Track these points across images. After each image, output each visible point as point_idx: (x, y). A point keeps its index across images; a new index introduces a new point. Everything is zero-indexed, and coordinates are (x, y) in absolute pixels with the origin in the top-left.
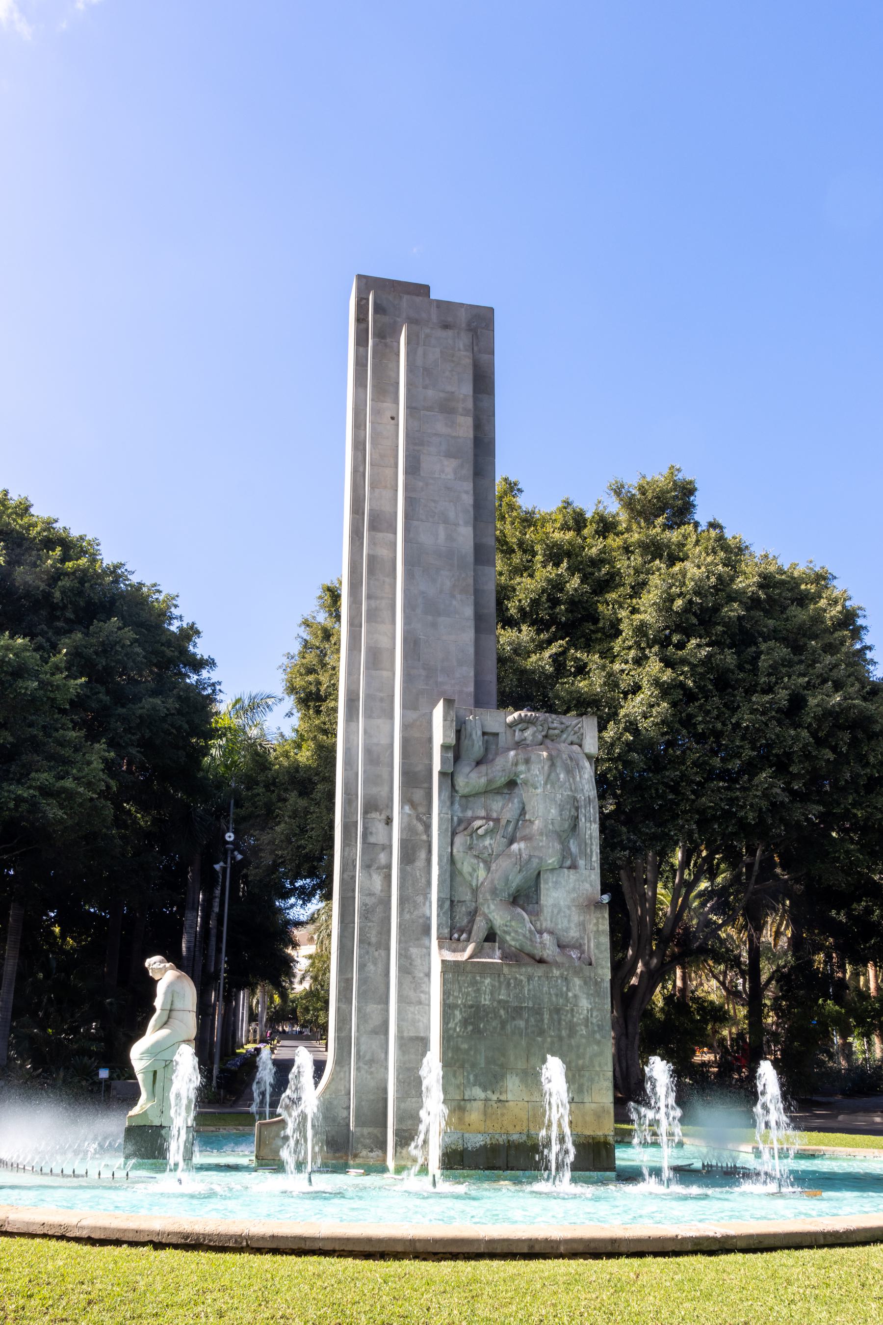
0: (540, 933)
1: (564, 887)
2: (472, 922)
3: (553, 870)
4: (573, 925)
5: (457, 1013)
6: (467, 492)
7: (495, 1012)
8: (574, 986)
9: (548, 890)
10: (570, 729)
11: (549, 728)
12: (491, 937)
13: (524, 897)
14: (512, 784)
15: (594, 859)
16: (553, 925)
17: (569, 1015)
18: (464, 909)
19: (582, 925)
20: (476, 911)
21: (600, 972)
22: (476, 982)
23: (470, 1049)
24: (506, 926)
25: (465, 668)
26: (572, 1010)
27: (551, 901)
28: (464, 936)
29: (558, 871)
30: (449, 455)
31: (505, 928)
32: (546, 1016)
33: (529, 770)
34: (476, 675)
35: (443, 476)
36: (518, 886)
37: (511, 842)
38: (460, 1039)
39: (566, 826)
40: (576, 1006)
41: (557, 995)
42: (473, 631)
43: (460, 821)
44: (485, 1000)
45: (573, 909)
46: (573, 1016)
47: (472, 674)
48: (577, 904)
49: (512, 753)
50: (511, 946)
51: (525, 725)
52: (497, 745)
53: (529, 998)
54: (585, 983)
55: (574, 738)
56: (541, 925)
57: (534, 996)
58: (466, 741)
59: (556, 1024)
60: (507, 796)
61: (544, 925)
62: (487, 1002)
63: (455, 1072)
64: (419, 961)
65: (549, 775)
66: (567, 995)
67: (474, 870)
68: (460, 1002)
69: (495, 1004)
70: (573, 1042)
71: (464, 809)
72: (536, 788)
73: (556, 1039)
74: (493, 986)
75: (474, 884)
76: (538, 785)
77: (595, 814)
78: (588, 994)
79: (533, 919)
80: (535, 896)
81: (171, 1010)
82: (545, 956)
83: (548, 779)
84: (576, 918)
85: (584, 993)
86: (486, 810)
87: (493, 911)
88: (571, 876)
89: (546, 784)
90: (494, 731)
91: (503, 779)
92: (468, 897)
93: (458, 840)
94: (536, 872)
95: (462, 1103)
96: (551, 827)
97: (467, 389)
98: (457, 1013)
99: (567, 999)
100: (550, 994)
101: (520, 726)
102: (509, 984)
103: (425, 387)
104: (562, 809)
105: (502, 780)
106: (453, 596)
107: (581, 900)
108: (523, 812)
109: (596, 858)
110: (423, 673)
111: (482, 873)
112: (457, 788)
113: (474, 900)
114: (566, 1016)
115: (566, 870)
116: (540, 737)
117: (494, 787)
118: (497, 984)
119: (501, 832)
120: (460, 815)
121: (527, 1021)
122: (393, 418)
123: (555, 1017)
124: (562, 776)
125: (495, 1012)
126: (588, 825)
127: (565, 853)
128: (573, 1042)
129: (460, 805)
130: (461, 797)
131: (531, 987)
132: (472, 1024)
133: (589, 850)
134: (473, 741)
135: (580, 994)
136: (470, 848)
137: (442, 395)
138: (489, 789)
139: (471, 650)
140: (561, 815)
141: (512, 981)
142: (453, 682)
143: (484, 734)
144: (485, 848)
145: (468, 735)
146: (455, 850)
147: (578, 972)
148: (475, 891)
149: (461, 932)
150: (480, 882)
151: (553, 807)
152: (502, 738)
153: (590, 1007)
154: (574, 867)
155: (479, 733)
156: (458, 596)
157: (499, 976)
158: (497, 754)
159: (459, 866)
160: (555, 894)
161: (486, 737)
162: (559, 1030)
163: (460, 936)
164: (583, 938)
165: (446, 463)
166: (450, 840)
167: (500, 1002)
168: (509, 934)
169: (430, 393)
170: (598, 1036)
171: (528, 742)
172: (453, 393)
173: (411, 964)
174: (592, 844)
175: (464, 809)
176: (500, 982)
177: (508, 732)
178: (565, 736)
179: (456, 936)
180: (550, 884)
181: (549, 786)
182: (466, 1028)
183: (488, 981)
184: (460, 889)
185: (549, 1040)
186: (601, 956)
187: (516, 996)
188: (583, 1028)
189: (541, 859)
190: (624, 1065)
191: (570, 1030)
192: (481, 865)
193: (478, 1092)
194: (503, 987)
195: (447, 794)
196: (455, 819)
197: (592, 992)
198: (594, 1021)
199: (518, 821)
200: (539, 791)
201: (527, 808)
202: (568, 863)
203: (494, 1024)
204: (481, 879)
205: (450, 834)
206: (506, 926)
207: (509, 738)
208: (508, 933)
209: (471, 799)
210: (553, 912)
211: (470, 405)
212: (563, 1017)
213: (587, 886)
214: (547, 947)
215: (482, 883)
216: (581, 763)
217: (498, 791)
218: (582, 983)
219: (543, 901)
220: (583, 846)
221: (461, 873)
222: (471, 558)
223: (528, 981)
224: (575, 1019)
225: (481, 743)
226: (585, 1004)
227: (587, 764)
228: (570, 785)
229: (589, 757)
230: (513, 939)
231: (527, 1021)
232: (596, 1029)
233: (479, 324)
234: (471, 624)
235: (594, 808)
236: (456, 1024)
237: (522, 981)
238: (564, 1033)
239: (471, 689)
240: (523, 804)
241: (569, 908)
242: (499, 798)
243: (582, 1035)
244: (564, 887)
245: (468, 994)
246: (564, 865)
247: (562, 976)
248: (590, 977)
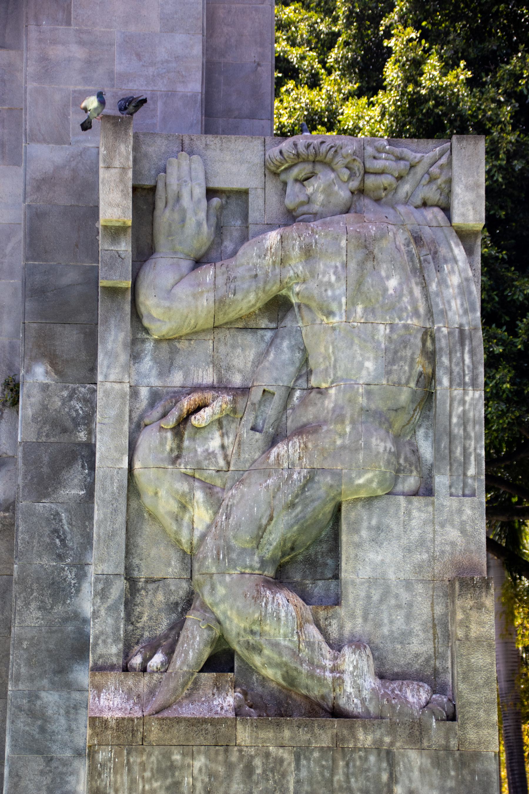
0: (336, 646)
1: (399, 538)
2: (178, 626)
3: (370, 500)
4: (416, 627)
8: (409, 769)
9: (358, 545)
11: (366, 172)
12: (221, 660)
13: (307, 564)
14: (279, 307)
15: (471, 471)
16: (369, 627)
19: (441, 629)
20: (189, 601)
21: (472, 735)
22: (172, 767)
24: (252, 632)
25: (180, 37)
27: (365, 573)
28: (158, 659)
29: (382, 503)
31: (250, 638)
37: (273, 442)
43: (155, 397)
45: (419, 588)
47: (197, 50)
48: (428, 576)
50: (265, 679)
54: (438, 762)
55: (432, 193)
56: (341, 627)
58: (167, 213)
60: (269, 335)
61: (348, 627)
64: (63, 721)
65: (360, 283)
67: (184, 507)
71: (165, 368)
72: (330, 313)
75: (184, 539)
76: (334, 307)
77: (474, 367)
79: (322, 614)
80: (330, 561)
82: (342, 702)
84: (423, 609)
87: (223, 600)
88: (415, 513)
89: (352, 303)
90: (236, 185)
92: (173, 569)
93: (148, 441)
94: (329, 508)
96: (362, 401)
101: (295, 172)
102: (249, 770)
104: (392, 356)
105: (249, 300)
107: (438, 567)
108: (305, 369)
110: (78, 53)
111: (201, 515)
112: (146, 323)
113: (186, 576)
115: (402, 499)
116: (343, 194)
117: (232, 314)
118: (221, 769)
120: (155, 382)
124: (393, 283)
126: (458, 392)
127: (404, 460)
129: (155, 359)
130: (158, 341)
131: (304, 773)
133: (458, 451)
134: (183, 211)
138: (221, 319)
140: (389, 373)
141: (258, 762)
142: (151, 71)
144: (210, 455)
145: (171, 196)
146: (137, 465)
147: (417, 733)
148: (189, 559)
149: (152, 648)
150: (197, 534)
151: (371, 355)
154: (426, 490)
155: (200, 192)
157: (226, 751)
158: (244, 238)
159: (147, 500)
160: (374, 556)
161: (216, 201)
163: (146, 660)
164: (443, 657)
166: (126, 443)
171: (316, 207)
173: (43, 730)
174: (467, 437)
175: (165, 368)
176: (230, 767)
177: (269, 185)
179: (137, 661)
180: (364, 533)
181: (359, 309)
183: (200, 762)
186: (474, 698)
189: (337, 475)
192: (199, 495)
194: (237, 774)
195: (121, 336)
196: (144, 392)
199: (290, 391)
200: (335, 320)
201: (312, 362)
202: (411, 482)
204: (200, 527)
205: (126, 427)
206: (252, 632)
207: (273, 199)
208: (257, 649)
209: (182, 345)
210: (369, 597)
214: (355, 681)
215: (203, 537)
216: (443, 251)
217: (245, 325)
218: (427, 762)
223: (298, 760)
225: (202, 215)
227: (459, 252)
229: (464, 236)
230: (270, 663)
235: (472, 352)
237: (281, 761)
239: (195, 86)
240: (304, 350)
241: (408, 585)
242: (248, 338)
244: (399, 538)
246: (400, 488)
247: (378, 746)
248: (447, 748)
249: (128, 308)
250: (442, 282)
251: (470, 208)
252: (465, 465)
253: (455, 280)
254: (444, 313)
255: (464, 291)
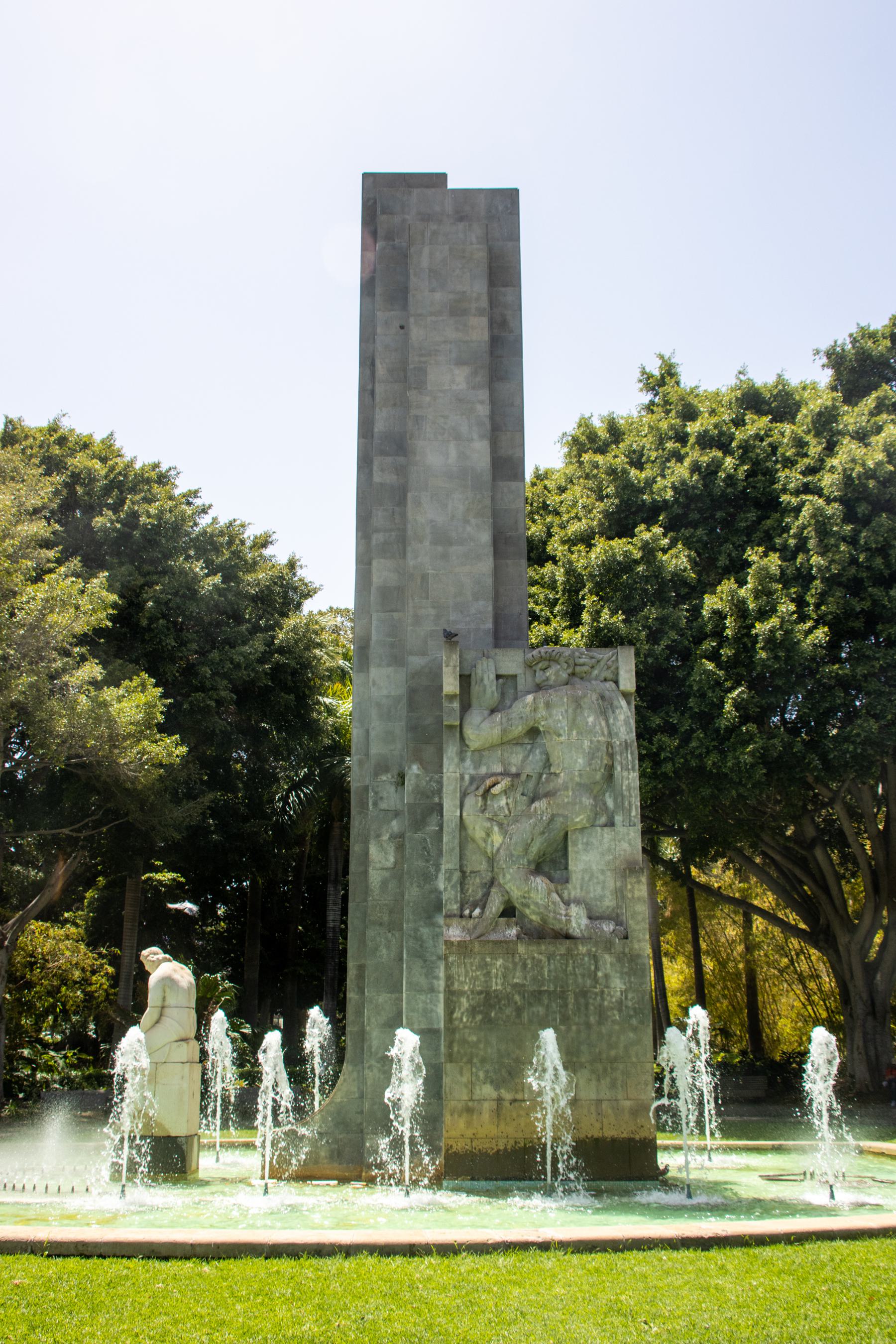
2: (487, 895)
3: (583, 830)
4: (608, 893)
5: (464, 1000)
6: (482, 402)
7: (509, 998)
8: (605, 964)
10: (602, 663)
12: (509, 911)
13: (552, 862)
14: (534, 733)
15: (633, 813)
16: (583, 894)
17: (599, 998)
18: (478, 880)
22: (486, 964)
23: (479, 1041)
25: (481, 603)
26: (602, 992)
27: (581, 866)
28: (477, 911)
30: (460, 362)
32: (571, 1000)
33: (551, 715)
34: (496, 608)
35: (454, 387)
36: (539, 850)
37: (533, 800)
38: (467, 1031)
39: (598, 776)
40: (607, 987)
41: (583, 976)
42: (491, 559)
44: (496, 985)
45: (609, 873)
46: (603, 999)
49: (530, 698)
51: (546, 663)
52: (516, 688)
53: (550, 981)
54: (619, 960)
55: (608, 674)
57: (556, 978)
59: (583, 1008)
60: (529, 747)
62: (499, 987)
63: (461, 1069)
65: (574, 720)
66: (596, 975)
67: (488, 835)
68: (466, 988)
69: (509, 989)
70: (604, 1030)
71: (477, 765)
72: (559, 735)
73: (582, 1027)
74: (506, 968)
75: (489, 851)
76: (562, 732)
78: (622, 973)
79: (559, 887)
81: (163, 1007)
83: (573, 724)
84: (611, 884)
85: (616, 971)
86: (503, 764)
90: (511, 673)
91: (520, 728)
92: (484, 866)
93: (469, 802)
94: (562, 834)
95: (470, 1104)
97: (480, 287)
98: (464, 1000)
99: (595, 979)
100: (575, 974)
101: (540, 665)
102: (525, 966)
103: (432, 290)
105: (519, 729)
106: (466, 521)
107: (618, 862)
108: (548, 763)
109: (636, 812)
110: (432, 612)
111: (497, 838)
114: (595, 999)
115: (599, 829)
116: (564, 675)
117: (510, 737)
118: (510, 965)
119: (520, 789)
121: (548, 1007)
122: (402, 327)
123: (582, 1001)
125: (509, 998)
126: (625, 774)
127: (599, 807)
128: (604, 1030)
129: (472, 761)
130: (473, 751)
131: (552, 967)
132: (480, 1012)
133: (627, 803)
134: (485, 686)
135: (613, 974)
136: (483, 811)
137: (451, 296)
138: (505, 739)
139: (489, 581)
141: (529, 962)
143: (498, 677)
144: (501, 808)
146: (464, 814)
147: (608, 946)
148: (491, 860)
150: (495, 848)
152: (521, 681)
153: (624, 987)
154: (611, 824)
156: (473, 521)
160: (585, 858)
161: (501, 681)
162: (587, 1016)
163: (471, 912)
165: (457, 372)
167: (515, 986)
168: (529, 907)
169: (438, 296)
170: (634, 1022)
171: (551, 682)
172: (464, 292)
173: (421, 946)
174: (630, 796)
176: (515, 964)
178: (596, 672)
179: (467, 912)
180: (580, 846)
181: (574, 732)
182: (474, 1018)
183: (500, 962)
184: (474, 858)
185: (574, 1028)
187: (534, 979)
188: (616, 1012)
189: (565, 817)
190: (872, 1053)
191: (600, 1016)
192: (496, 829)
193: (488, 1090)
194: (519, 968)
196: (467, 777)
197: (626, 970)
198: (630, 1004)
199: (541, 775)
203: (508, 1011)
204: (496, 845)
209: (485, 753)
210: (583, 878)
211: (484, 303)
212: (591, 1001)
213: (625, 845)
214: (577, 920)
215: (498, 850)
216: (615, 703)
217: (517, 742)
218: (614, 960)
219: (572, 866)
220: (619, 800)
221: (473, 840)
222: (487, 477)
224: (606, 1003)
226: (618, 984)
227: (623, 703)
228: (602, 729)
229: (626, 695)
230: (534, 913)
231: (548, 1007)
232: (632, 1013)
233: (500, 209)
234: (490, 550)
235: (632, 754)
236: (462, 1014)
238: (593, 1019)
239: (489, 625)
240: (547, 754)
241: (603, 872)
242: (519, 749)
243: (614, 1022)
245: (476, 978)
247: (589, 953)
249: (458, 735)
250: (615, 719)
251: (628, 681)
252: (630, 811)
253: (622, 717)
254: (617, 734)
255: (626, 722)
